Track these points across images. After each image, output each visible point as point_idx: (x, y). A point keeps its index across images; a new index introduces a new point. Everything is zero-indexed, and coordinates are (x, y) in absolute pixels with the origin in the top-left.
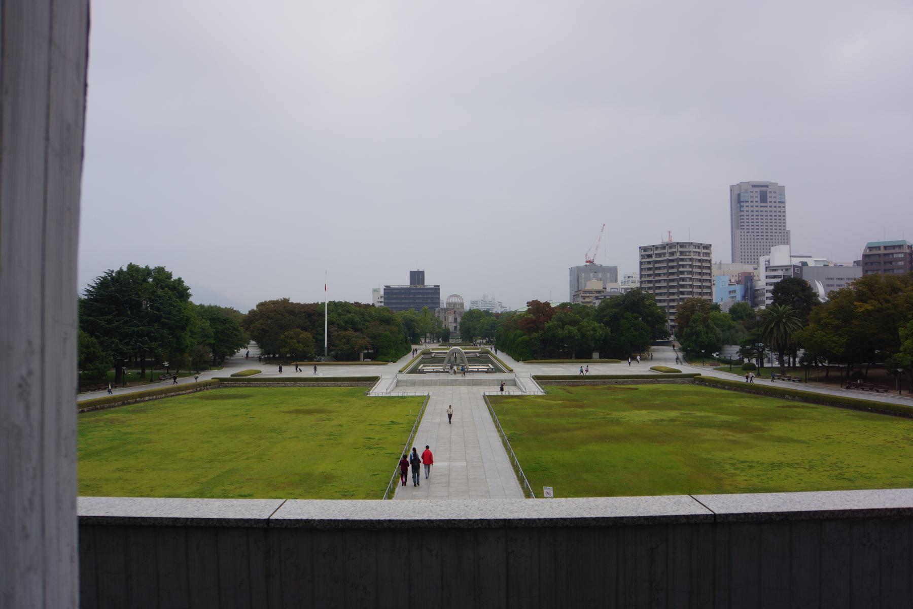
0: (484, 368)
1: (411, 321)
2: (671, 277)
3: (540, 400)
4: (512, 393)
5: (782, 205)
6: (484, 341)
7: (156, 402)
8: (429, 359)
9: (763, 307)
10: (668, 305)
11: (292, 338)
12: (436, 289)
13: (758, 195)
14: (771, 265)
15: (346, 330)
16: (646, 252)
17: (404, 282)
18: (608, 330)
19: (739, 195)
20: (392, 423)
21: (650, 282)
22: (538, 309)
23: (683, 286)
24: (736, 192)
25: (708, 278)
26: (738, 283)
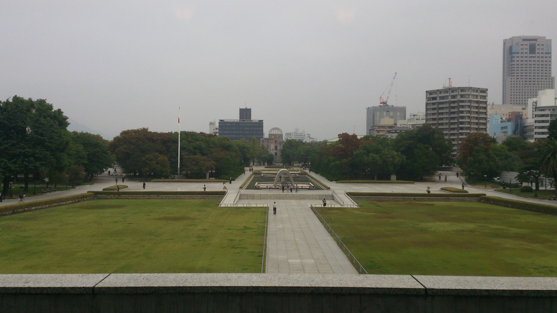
0: (306, 186)
1: (244, 148)
2: (452, 116)
3: (357, 212)
4: (333, 206)
5: (549, 55)
6: (301, 165)
7: (42, 211)
8: (258, 177)
9: (532, 141)
10: (456, 139)
11: (152, 160)
12: (261, 123)
13: (528, 47)
14: (538, 105)
15: (195, 154)
16: (431, 95)
17: (235, 117)
18: (404, 157)
19: (511, 48)
20: (246, 228)
21: (434, 119)
22: (347, 140)
23: (462, 123)
24: (508, 45)
25: (484, 116)
26: (509, 120)
